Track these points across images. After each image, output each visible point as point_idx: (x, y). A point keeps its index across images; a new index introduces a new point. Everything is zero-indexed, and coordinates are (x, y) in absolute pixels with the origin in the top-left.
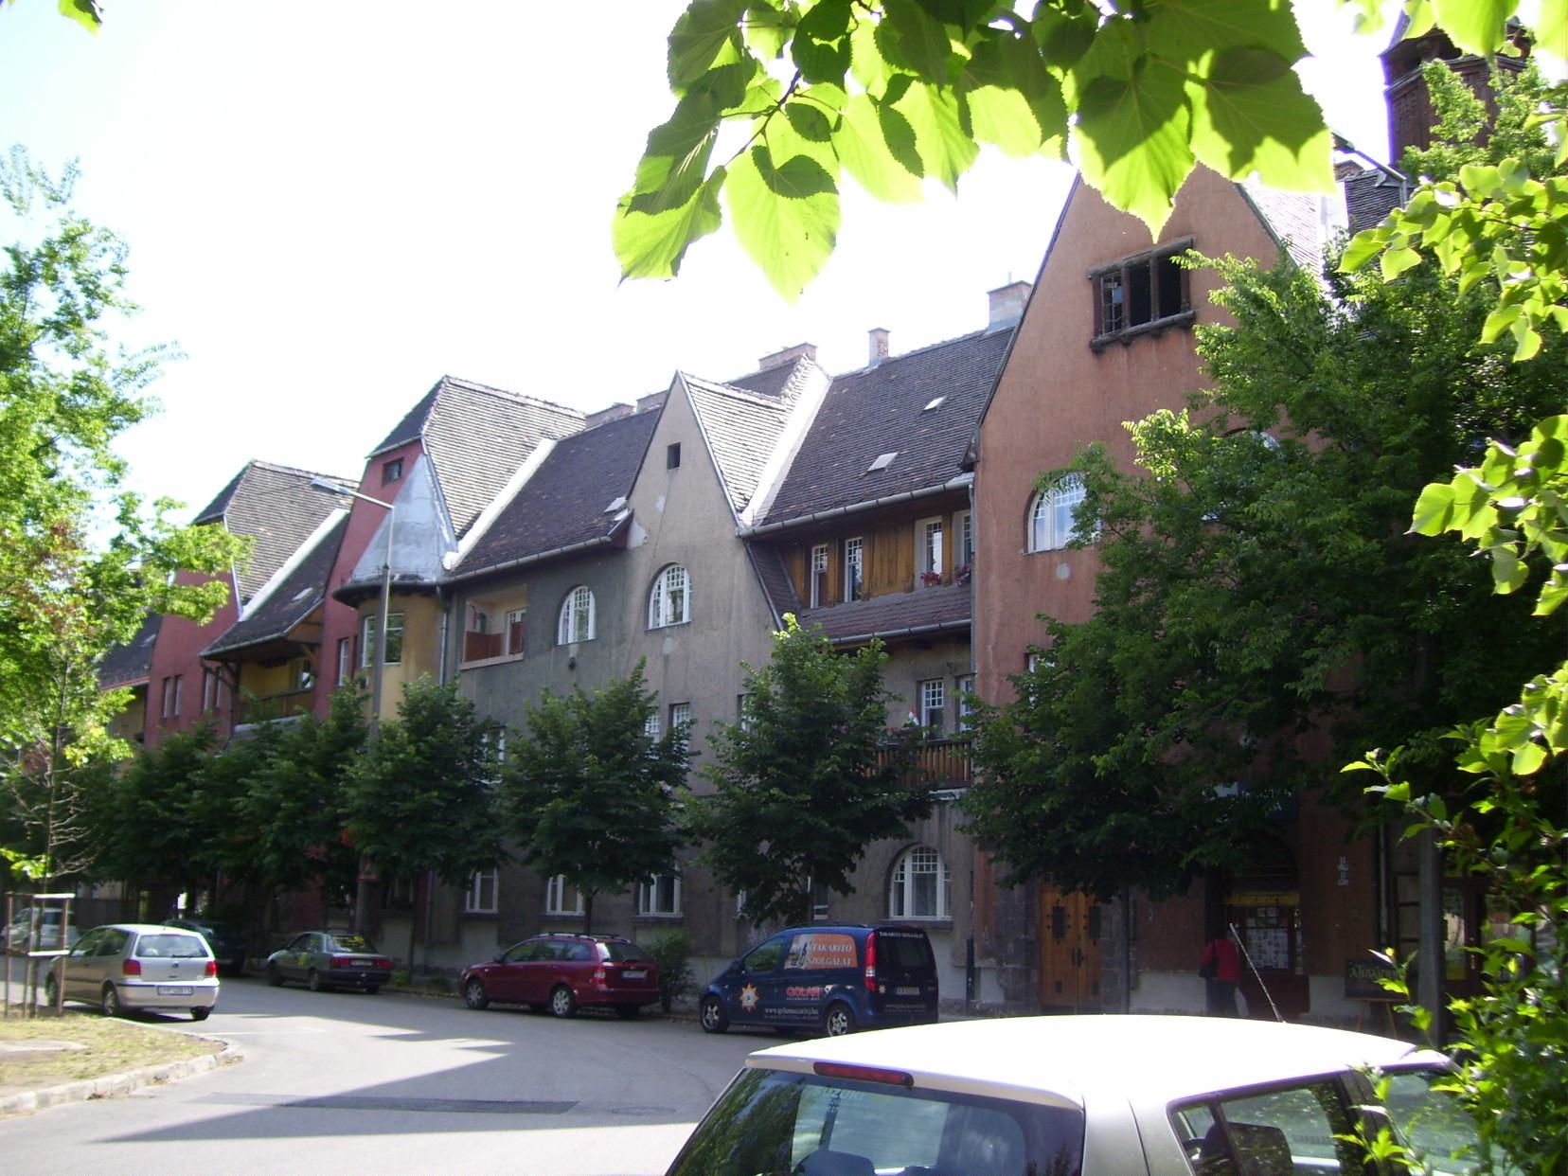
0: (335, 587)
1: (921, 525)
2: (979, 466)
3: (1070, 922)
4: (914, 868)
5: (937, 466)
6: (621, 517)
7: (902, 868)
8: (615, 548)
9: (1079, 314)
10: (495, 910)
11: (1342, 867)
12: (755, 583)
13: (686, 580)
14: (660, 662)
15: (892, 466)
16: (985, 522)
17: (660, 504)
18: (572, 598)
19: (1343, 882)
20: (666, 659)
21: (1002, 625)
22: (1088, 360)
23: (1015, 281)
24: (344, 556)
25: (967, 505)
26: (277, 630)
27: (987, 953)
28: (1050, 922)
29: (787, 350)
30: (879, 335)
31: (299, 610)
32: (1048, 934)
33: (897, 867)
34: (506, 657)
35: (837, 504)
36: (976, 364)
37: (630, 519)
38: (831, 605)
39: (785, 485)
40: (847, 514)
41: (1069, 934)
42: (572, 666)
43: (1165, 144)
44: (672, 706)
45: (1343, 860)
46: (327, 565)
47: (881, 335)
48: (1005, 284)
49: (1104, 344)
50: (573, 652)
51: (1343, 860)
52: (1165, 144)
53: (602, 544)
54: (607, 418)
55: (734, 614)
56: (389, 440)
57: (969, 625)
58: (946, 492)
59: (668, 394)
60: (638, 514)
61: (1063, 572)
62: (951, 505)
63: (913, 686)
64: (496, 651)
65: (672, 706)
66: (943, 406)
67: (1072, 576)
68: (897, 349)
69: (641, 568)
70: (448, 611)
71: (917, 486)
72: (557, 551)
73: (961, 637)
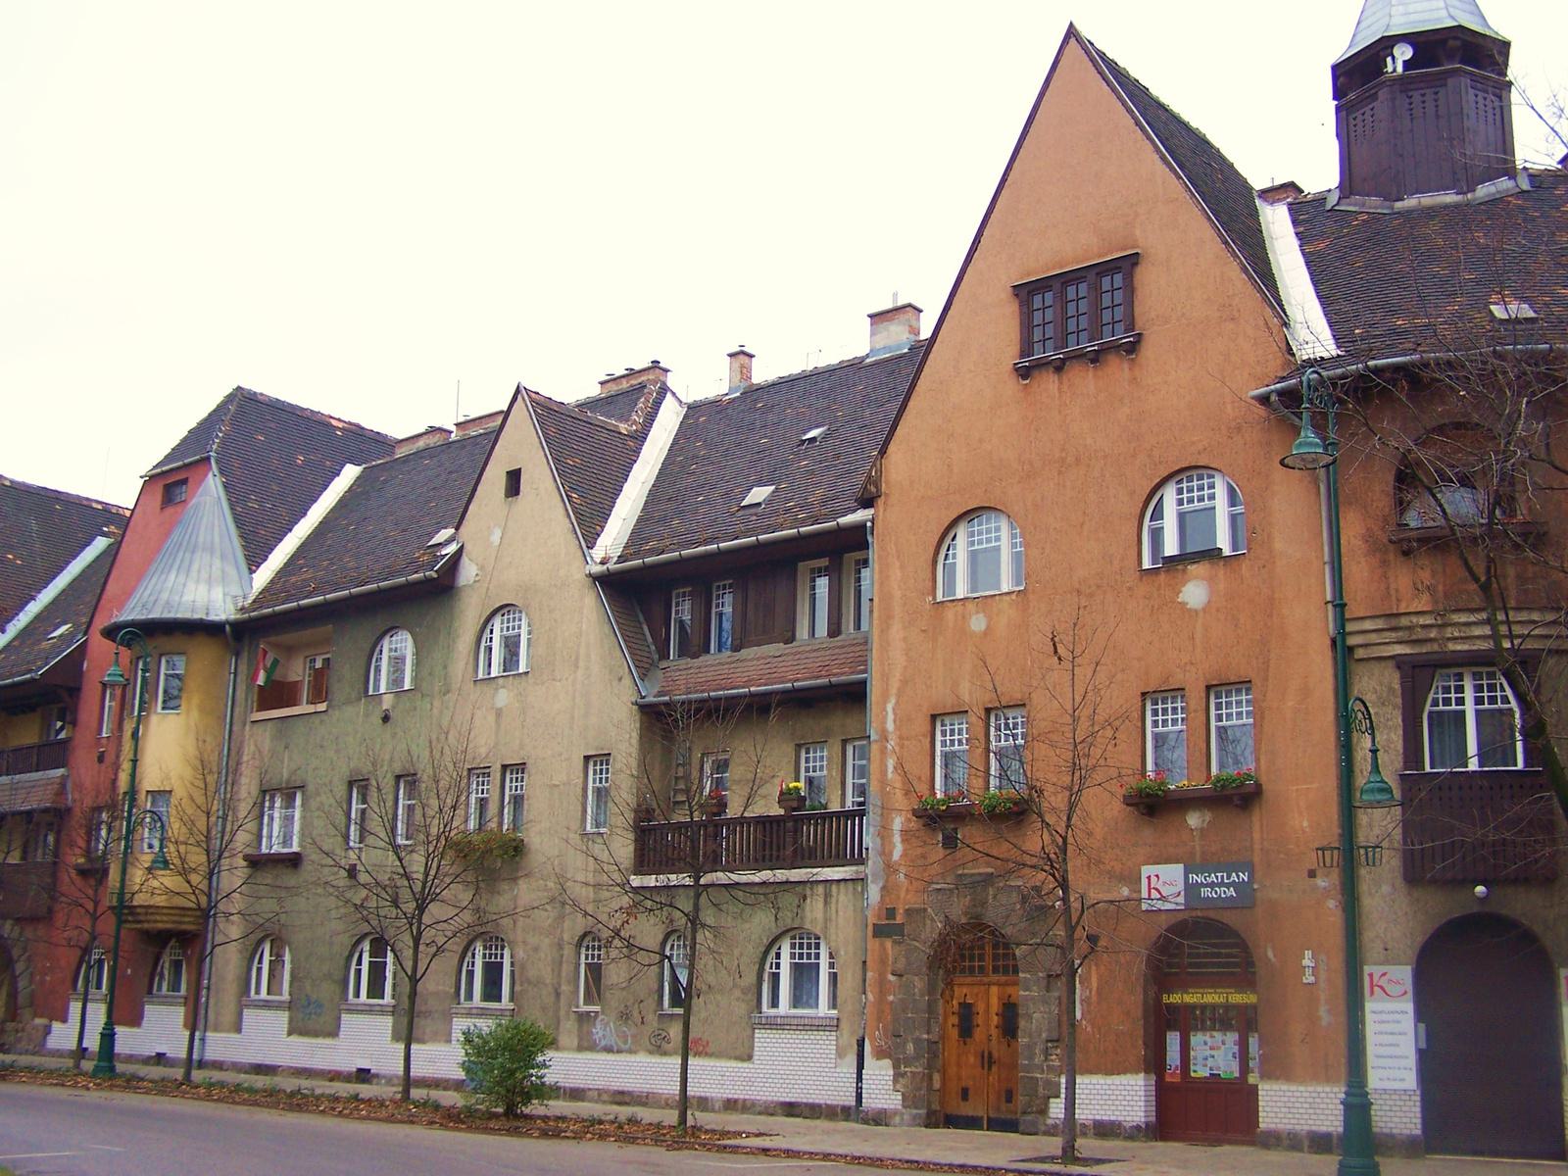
0: (101, 622)
1: (803, 567)
2: (880, 502)
3: (980, 1020)
4: (793, 955)
5: (824, 502)
6: (452, 548)
7: (778, 956)
8: (438, 589)
9: (998, 332)
10: (286, 997)
11: (1306, 962)
12: (607, 629)
13: (524, 623)
14: (491, 718)
15: (769, 501)
16: (884, 577)
17: (496, 538)
18: (386, 643)
19: (1309, 978)
20: (499, 713)
21: (904, 682)
22: (1012, 386)
23: (900, 303)
24: (112, 588)
25: (864, 545)
26: (30, 671)
27: (880, 1054)
28: (954, 1020)
29: (632, 373)
30: (741, 356)
31: (56, 649)
32: (954, 1033)
33: (773, 954)
34: (304, 708)
35: (706, 542)
36: (875, 392)
37: (460, 552)
38: (695, 656)
39: (640, 520)
40: (720, 552)
41: (979, 1034)
42: (386, 719)
43: (1430, 105)
44: (505, 767)
45: (1308, 954)
46: (90, 598)
47: (743, 359)
48: (889, 305)
49: (1041, 365)
50: (387, 702)
51: (1308, 954)
52: (1430, 105)
53: (428, 581)
54: (421, 444)
55: (581, 664)
56: (168, 458)
57: (864, 683)
58: (841, 530)
59: (507, 414)
60: (468, 547)
61: (978, 623)
62: (844, 550)
63: (790, 749)
64: (293, 702)
65: (505, 767)
66: (825, 436)
67: (988, 627)
68: (763, 373)
69: (470, 611)
70: (237, 654)
71: (803, 522)
72: (373, 586)
73: (854, 696)
